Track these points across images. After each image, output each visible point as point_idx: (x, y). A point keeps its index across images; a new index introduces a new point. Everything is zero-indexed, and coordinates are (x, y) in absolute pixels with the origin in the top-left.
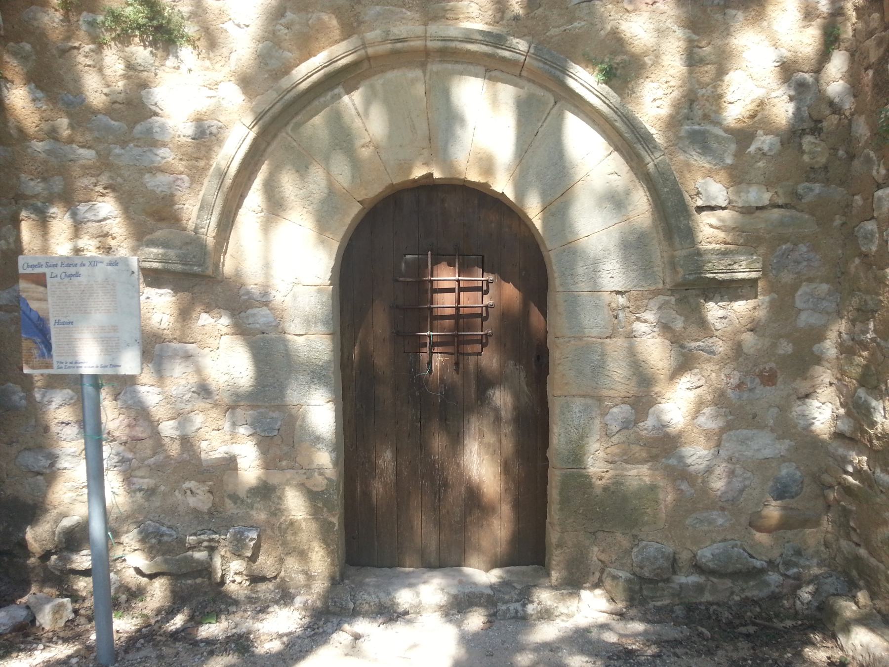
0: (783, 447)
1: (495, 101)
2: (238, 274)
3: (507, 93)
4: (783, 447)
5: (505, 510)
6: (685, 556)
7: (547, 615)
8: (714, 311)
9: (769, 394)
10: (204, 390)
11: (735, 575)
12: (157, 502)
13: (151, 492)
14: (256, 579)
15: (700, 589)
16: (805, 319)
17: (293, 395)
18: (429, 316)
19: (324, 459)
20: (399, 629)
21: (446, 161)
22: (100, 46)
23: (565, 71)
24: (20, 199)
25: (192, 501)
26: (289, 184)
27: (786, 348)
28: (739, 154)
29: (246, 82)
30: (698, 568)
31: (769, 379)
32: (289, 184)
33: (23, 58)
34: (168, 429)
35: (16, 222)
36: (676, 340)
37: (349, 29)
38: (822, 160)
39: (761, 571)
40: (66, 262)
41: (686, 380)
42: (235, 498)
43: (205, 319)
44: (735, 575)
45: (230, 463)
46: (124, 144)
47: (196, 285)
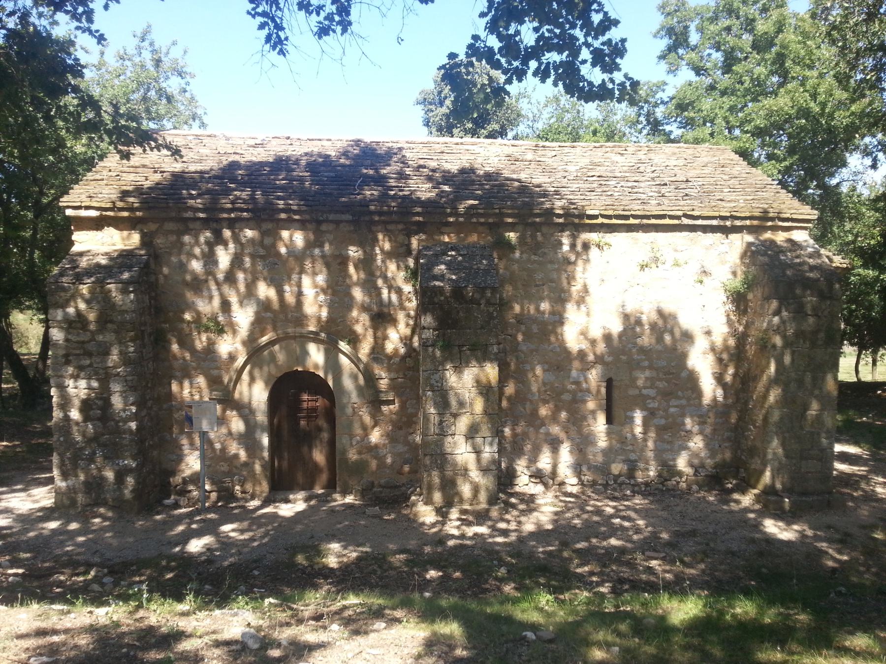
0: (406, 448)
1: (319, 349)
2: (240, 399)
3: (322, 347)
4: (406, 448)
5: (326, 470)
6: (376, 483)
7: (335, 500)
8: (385, 408)
9: (402, 433)
10: (230, 433)
11: (391, 487)
12: (211, 469)
13: (209, 466)
14: (243, 492)
15: (381, 492)
16: (410, 411)
17: (257, 435)
18: (301, 410)
19: (266, 454)
20: (591, 290)
21: (304, 366)
22: (199, 333)
23: (337, 343)
24: (172, 377)
25: (222, 469)
26: (257, 373)
27: (405, 419)
28: (389, 363)
29: (244, 343)
30: (380, 486)
31: (400, 428)
32: (257, 373)
33: (175, 337)
34: (218, 446)
35: (170, 384)
36: (373, 416)
37: (275, 329)
38: (412, 365)
39: (400, 486)
40: (198, 402)
41: (377, 429)
42: (236, 467)
43: (228, 412)
44: (391, 487)
45: (236, 456)
46: (204, 361)
47: (551, 641)
